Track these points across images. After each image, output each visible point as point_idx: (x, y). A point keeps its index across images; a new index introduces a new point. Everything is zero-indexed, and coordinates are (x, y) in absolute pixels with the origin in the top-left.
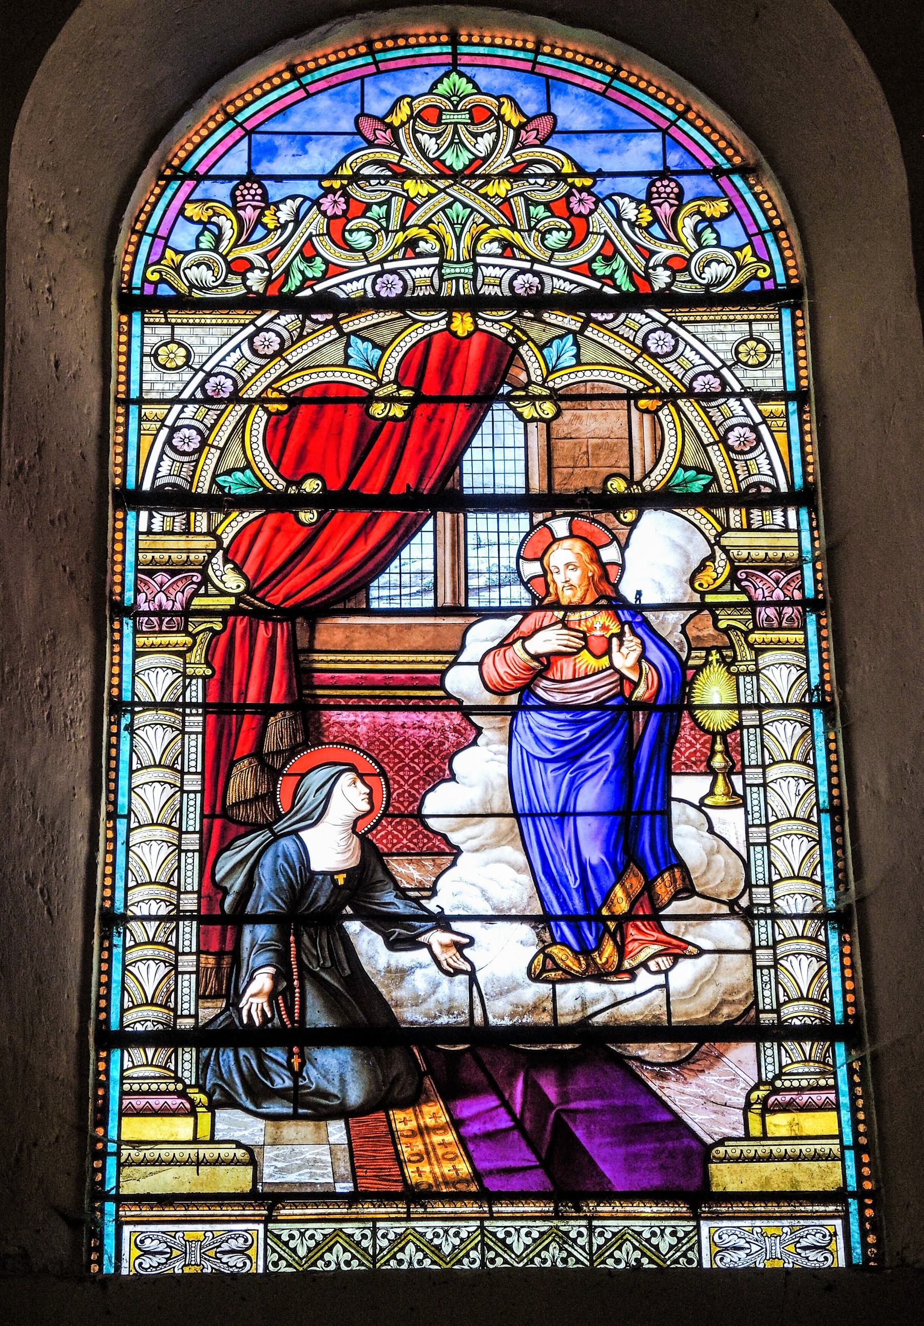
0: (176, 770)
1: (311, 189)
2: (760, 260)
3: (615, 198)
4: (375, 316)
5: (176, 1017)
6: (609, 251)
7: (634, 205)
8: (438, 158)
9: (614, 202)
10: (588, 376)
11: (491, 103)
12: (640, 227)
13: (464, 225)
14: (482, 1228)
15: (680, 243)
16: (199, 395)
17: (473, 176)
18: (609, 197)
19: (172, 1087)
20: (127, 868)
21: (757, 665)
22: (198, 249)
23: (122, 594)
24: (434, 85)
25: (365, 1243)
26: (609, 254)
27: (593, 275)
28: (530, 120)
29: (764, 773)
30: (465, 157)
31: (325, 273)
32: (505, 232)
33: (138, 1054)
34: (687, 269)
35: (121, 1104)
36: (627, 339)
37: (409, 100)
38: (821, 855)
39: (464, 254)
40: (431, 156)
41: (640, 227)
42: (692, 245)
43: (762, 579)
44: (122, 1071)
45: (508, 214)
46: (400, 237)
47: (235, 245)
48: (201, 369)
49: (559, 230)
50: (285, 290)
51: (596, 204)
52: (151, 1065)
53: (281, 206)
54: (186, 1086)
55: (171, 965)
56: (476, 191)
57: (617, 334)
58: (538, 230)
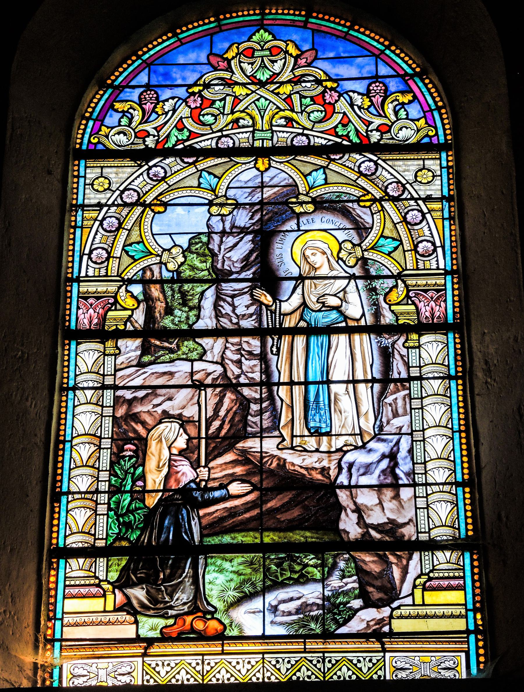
2: (430, 126)
3: (351, 94)
4: (216, 160)
7: (360, 97)
8: (252, 75)
9: (349, 95)
10: (331, 189)
11: (282, 45)
12: (363, 108)
16: (120, 202)
17: (272, 83)
18: (346, 93)
19: (92, 582)
21: (419, 342)
22: (120, 125)
26: (345, 123)
27: (337, 135)
33: (73, 562)
35: (64, 592)
36: (350, 168)
37: (237, 45)
39: (266, 127)
40: (249, 74)
42: (393, 118)
43: (424, 297)
44: (65, 574)
47: (140, 123)
49: (318, 111)
50: (166, 146)
51: (339, 97)
52: (82, 570)
53: (166, 103)
54: (101, 581)
57: (345, 165)
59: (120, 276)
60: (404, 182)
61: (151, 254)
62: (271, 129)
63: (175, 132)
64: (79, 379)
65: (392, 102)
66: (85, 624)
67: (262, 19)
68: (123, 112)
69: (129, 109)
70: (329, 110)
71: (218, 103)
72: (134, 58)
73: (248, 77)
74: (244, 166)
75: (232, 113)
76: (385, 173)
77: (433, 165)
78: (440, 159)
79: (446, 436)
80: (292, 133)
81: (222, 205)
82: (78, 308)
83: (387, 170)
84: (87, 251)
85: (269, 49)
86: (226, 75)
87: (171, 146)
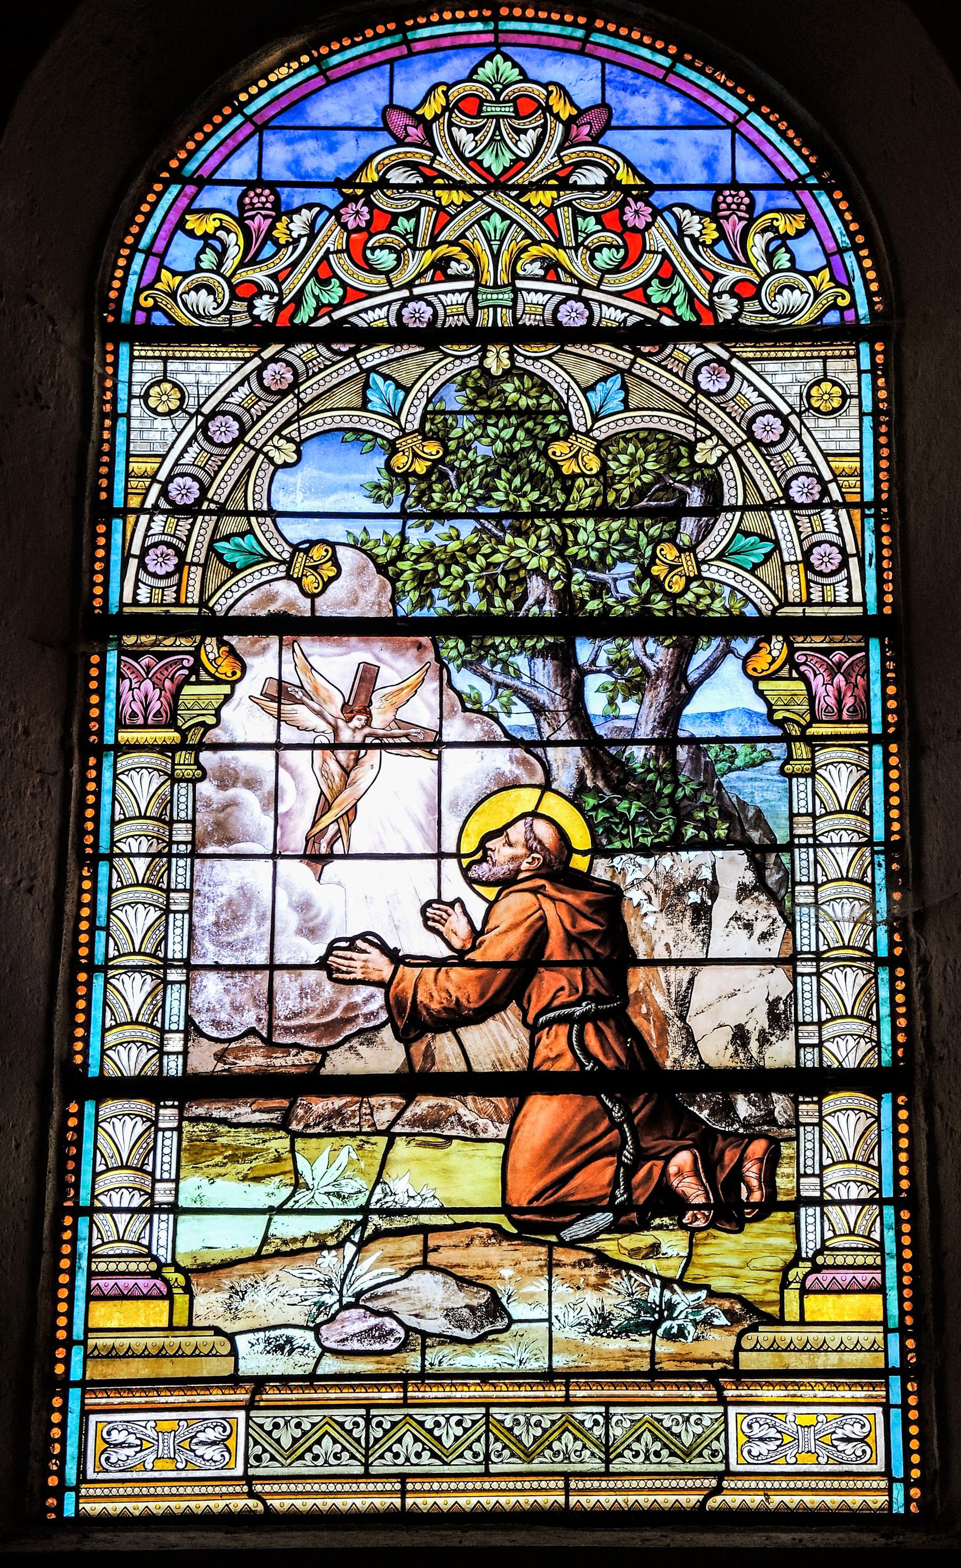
0: (155, 1028)
1: (329, 198)
2: (839, 285)
6: (665, 275)
11: (538, 92)
12: (704, 244)
14: (487, 1415)
18: (669, 208)
19: (143, 1267)
20: (96, 1148)
22: (199, 269)
24: (474, 71)
25: (356, 1433)
26: (667, 274)
28: (581, 112)
29: (816, 892)
30: (506, 159)
31: (342, 298)
32: (548, 249)
34: (757, 296)
38: (879, 1135)
39: (503, 278)
42: (763, 268)
44: (91, 1248)
46: (429, 257)
48: (199, 412)
49: (610, 247)
53: (295, 217)
54: (161, 1266)
58: (587, 248)
61: (269, 558)
62: (512, 284)
64: (120, 831)
66: (130, 1354)
68: (206, 236)
69: (217, 229)
70: (633, 245)
71: (402, 221)
74: (457, 362)
75: (434, 245)
76: (747, 391)
77: (845, 371)
80: (554, 293)
82: (121, 676)
84: (136, 550)
86: (423, 156)
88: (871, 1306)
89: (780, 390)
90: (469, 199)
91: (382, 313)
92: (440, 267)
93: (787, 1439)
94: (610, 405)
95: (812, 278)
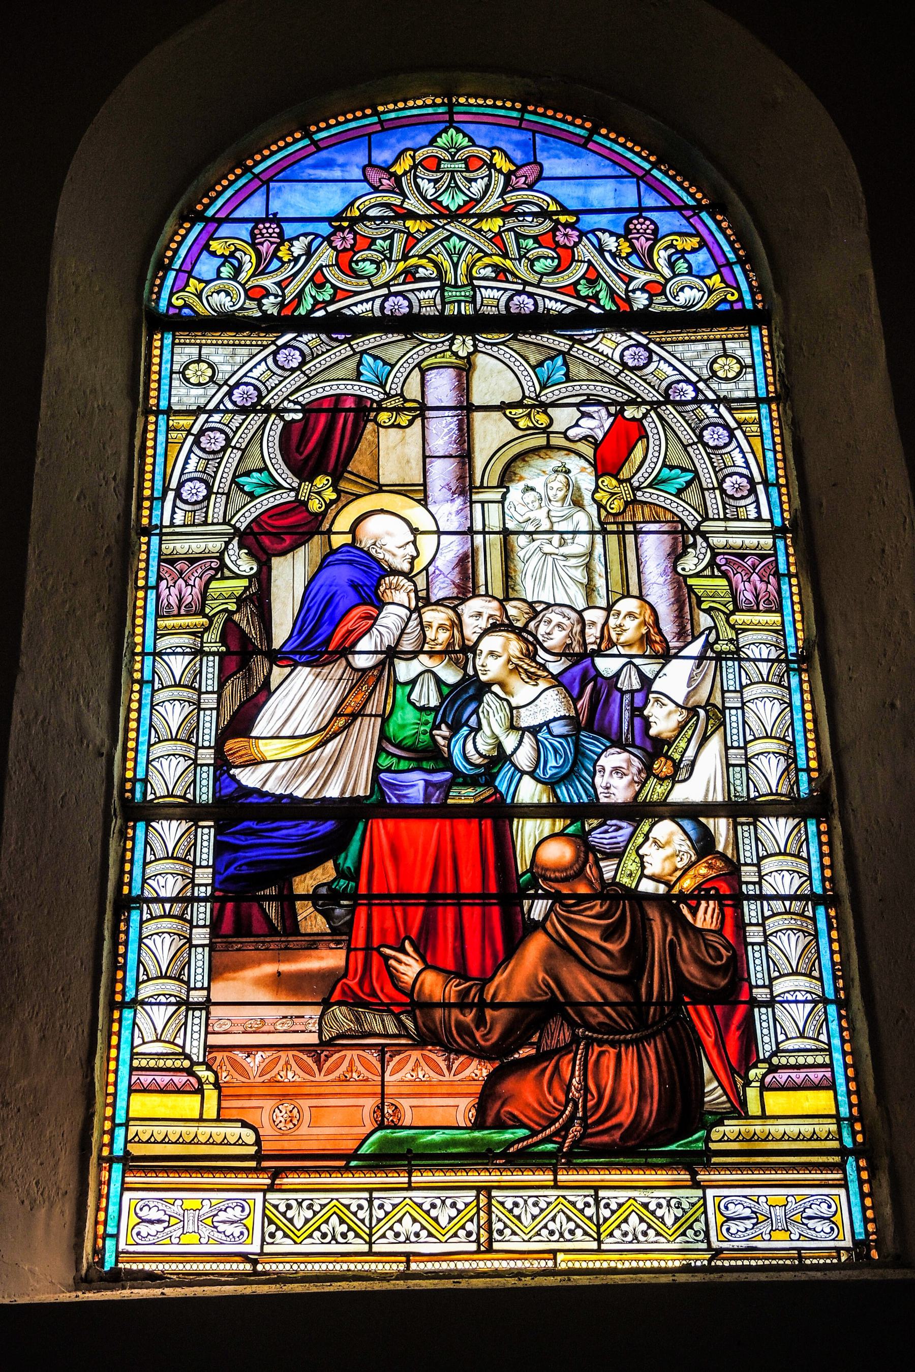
1: (324, 229)
2: (728, 286)
3: (599, 234)
5: (189, 989)
6: (592, 276)
7: (614, 239)
8: (435, 200)
11: (485, 154)
13: (460, 255)
15: (656, 270)
16: (230, 406)
17: (468, 216)
18: (593, 232)
19: (178, 1064)
22: (219, 277)
23: (157, 303)
27: (579, 297)
30: (460, 199)
32: (497, 260)
34: (663, 293)
39: (462, 280)
41: (621, 258)
42: (667, 273)
43: (740, 566)
44: (133, 1048)
45: (501, 246)
46: (401, 266)
49: (546, 258)
51: (580, 238)
53: (295, 243)
54: (193, 1064)
55: (185, 937)
56: (470, 227)
58: (528, 258)
59: (228, 524)
60: (694, 378)
62: (471, 284)
63: (310, 290)
65: (666, 249)
67: (451, 113)
70: (565, 258)
72: (238, 171)
73: (428, 202)
78: (750, 339)
79: (798, 873)
81: (398, 410)
83: (666, 361)
84: (174, 485)
85: (466, 161)
86: (396, 200)
87: (303, 313)
88: (821, 1101)
89: (688, 364)
90: (431, 226)
91: (368, 306)
92: (410, 274)
93: (761, 1218)
94: (556, 377)
95: (706, 280)
